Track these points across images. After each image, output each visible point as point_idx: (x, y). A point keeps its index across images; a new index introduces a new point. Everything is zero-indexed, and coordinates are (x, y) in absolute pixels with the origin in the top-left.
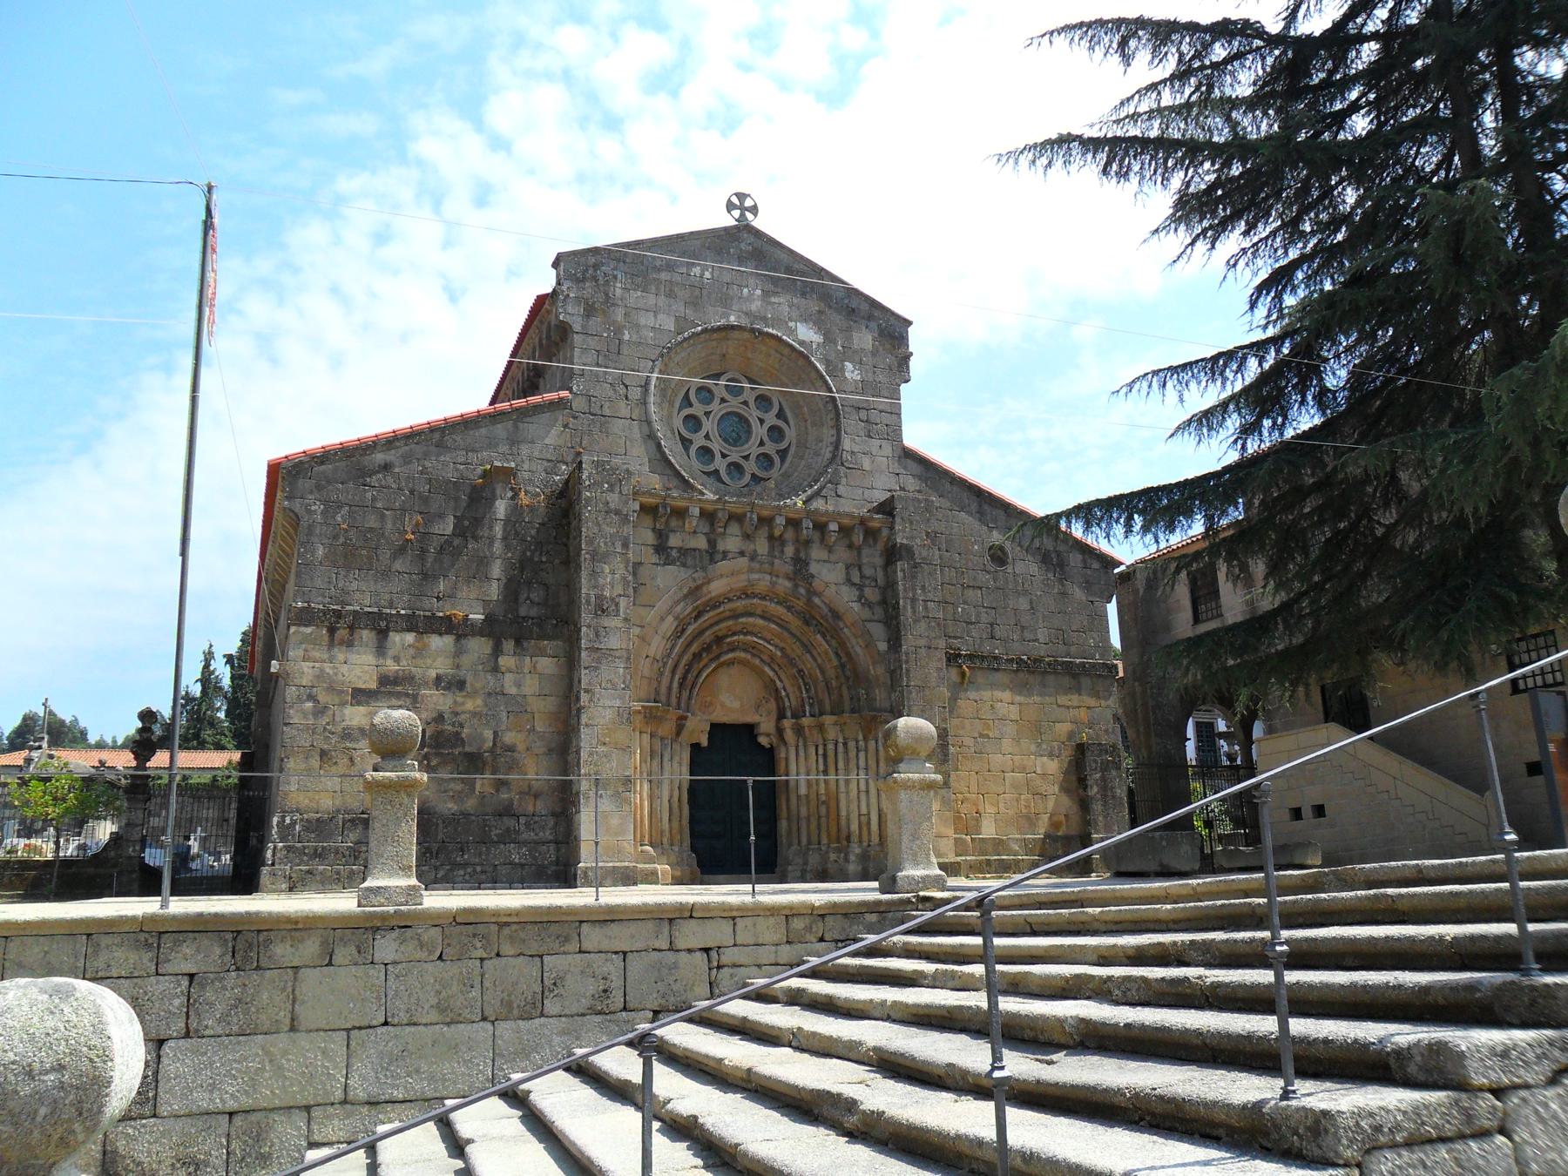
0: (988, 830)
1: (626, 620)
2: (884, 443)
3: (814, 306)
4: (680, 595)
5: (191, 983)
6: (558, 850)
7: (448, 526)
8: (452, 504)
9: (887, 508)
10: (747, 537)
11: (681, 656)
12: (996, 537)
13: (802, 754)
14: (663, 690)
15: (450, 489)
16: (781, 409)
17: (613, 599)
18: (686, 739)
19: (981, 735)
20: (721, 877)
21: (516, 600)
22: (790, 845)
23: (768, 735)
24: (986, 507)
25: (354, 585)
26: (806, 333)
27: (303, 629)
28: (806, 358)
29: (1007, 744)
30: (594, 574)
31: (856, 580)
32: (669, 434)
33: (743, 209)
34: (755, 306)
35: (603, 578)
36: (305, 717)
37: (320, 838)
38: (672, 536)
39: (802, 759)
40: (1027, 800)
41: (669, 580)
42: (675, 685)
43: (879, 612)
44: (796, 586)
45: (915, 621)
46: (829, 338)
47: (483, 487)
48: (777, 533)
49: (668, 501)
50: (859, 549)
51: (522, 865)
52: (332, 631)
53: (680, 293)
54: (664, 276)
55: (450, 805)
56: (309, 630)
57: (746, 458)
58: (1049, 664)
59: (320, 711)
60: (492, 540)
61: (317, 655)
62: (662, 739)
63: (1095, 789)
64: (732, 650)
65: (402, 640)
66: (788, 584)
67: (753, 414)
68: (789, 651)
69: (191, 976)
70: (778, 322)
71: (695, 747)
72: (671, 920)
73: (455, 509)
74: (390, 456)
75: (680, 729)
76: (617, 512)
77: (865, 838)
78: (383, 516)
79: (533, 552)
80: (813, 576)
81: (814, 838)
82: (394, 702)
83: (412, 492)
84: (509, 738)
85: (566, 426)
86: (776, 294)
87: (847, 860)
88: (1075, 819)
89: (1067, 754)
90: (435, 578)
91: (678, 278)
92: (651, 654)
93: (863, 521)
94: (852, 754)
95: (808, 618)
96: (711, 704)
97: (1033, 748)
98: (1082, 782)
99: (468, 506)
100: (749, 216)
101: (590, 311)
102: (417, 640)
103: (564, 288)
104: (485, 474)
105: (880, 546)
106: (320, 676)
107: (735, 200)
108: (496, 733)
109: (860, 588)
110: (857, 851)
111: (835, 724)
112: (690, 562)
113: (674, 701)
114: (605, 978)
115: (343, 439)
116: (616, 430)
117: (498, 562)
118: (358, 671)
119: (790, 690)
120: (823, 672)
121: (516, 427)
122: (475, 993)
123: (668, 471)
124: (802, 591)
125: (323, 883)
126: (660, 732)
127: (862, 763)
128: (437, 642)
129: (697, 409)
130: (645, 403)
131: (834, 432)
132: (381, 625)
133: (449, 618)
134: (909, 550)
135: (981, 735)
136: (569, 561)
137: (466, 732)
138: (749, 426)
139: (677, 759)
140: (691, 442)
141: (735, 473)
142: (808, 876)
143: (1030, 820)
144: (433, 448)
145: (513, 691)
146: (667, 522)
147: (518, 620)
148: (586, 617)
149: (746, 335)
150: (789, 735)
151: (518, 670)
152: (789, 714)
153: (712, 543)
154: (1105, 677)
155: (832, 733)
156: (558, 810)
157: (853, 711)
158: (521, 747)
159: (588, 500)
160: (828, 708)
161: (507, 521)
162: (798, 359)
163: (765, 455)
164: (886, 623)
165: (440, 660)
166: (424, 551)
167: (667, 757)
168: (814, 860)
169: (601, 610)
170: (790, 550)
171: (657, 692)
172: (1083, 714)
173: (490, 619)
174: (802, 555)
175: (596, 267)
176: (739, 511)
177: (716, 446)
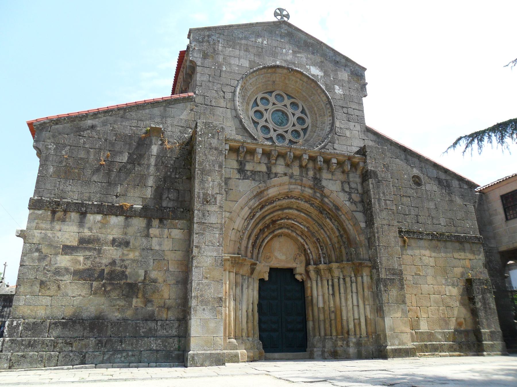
0: (424, 327)
1: (221, 207)
2: (356, 124)
3: (318, 59)
4: (252, 195)
6: (179, 341)
7: (124, 158)
8: (128, 146)
9: (362, 152)
10: (288, 165)
11: (253, 230)
12: (415, 171)
13: (320, 284)
14: (243, 248)
15: (126, 139)
17: (213, 196)
18: (256, 276)
19: (416, 274)
20: (276, 355)
21: (161, 198)
22: (314, 336)
23: (301, 274)
24: (409, 157)
25: (69, 188)
26: (315, 71)
27: (36, 211)
28: (315, 82)
29: (430, 279)
30: (202, 181)
31: (347, 189)
32: (246, 118)
34: (289, 57)
35: (208, 183)
36: (33, 261)
37: (34, 335)
38: (247, 164)
39: (320, 284)
40: (443, 310)
41: (245, 188)
42: (250, 245)
43: (360, 207)
45: (381, 211)
46: (326, 74)
47: (145, 138)
48: (304, 164)
49: (245, 145)
50: (348, 174)
51: (157, 351)
52: (54, 212)
53: (251, 50)
54: (243, 42)
55: (116, 314)
56: (40, 212)
57: (286, 132)
58: (448, 237)
60: (149, 166)
61: (43, 226)
62: (242, 276)
64: (281, 228)
66: (311, 191)
67: (289, 111)
68: (311, 228)
70: (300, 65)
71: (261, 281)
73: (129, 149)
74: (95, 122)
75: (253, 271)
76: (216, 149)
78: (88, 152)
79: (171, 173)
80: (324, 187)
81: (328, 332)
82: (190, 265)
83: (106, 140)
84: (154, 275)
85: (192, 110)
87: (348, 346)
88: (470, 320)
89: (462, 284)
90: (116, 185)
91: (251, 43)
92: (236, 228)
93: (349, 158)
94: (348, 285)
95: (322, 210)
96: (270, 257)
97: (444, 281)
98: (472, 300)
99: (137, 148)
101: (205, 56)
103: (193, 45)
104: (147, 132)
105: (359, 172)
106: (45, 238)
107: (278, 11)
108: (146, 272)
109: (350, 194)
110: (354, 340)
111: (338, 268)
112: (257, 178)
113: (249, 254)
115: (69, 112)
116: (218, 113)
117: (152, 177)
119: (312, 249)
120: (330, 240)
121: (165, 110)
123: (246, 134)
124: (318, 195)
125: (31, 363)
126: (241, 272)
127: (354, 290)
128: (115, 220)
129: (261, 108)
130: (234, 101)
131: (331, 118)
132: (82, 211)
133: (121, 207)
134: (375, 173)
135: (416, 274)
137: (128, 271)
139: (251, 287)
140: (258, 123)
142: (326, 355)
143: (446, 321)
144: (119, 119)
145: (157, 248)
146: (244, 157)
147: (161, 209)
148: (197, 205)
149: (285, 71)
150: (312, 274)
151: (161, 236)
152: (312, 263)
153: (269, 169)
154: (477, 243)
155: (336, 273)
156: (181, 317)
157: (348, 260)
158: (160, 280)
159: (200, 142)
160: (334, 259)
161: (158, 156)
162: (312, 82)
163: (296, 131)
164: (364, 213)
165: (115, 230)
166: (110, 171)
167: (245, 286)
169: (206, 201)
170: (311, 173)
171: (239, 249)
172: (467, 263)
173: (145, 208)
174: (318, 176)
175: (209, 36)
176: (283, 151)
177: (271, 126)
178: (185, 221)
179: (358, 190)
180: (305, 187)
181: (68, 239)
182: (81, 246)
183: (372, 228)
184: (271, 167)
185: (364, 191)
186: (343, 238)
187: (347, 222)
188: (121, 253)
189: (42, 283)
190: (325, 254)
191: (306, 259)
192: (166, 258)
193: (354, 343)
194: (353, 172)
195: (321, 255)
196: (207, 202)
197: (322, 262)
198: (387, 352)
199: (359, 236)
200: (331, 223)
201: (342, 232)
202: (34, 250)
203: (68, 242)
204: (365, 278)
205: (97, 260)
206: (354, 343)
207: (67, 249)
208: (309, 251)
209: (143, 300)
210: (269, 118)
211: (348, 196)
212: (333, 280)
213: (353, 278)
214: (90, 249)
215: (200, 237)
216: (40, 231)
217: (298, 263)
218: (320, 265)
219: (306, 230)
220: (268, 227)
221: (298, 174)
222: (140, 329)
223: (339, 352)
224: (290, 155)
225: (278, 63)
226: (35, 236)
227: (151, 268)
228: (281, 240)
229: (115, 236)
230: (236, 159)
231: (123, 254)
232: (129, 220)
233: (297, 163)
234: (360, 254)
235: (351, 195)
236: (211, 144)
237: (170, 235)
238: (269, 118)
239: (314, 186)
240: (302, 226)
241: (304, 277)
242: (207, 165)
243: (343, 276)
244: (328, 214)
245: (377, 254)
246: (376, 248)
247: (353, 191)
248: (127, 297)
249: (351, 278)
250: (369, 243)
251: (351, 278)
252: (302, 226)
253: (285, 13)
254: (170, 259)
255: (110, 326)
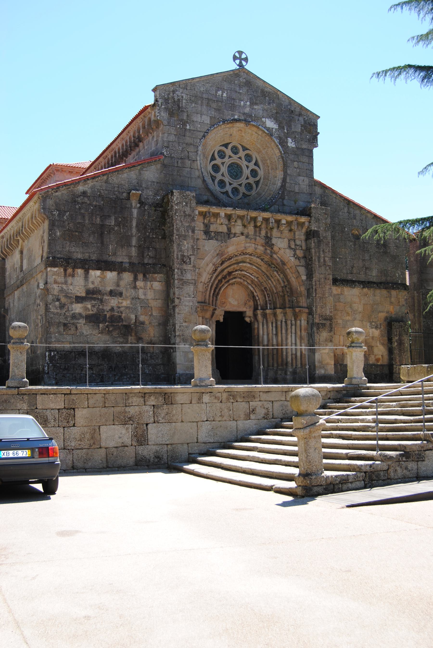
5: (154, 408)
10: (244, 226)
11: (214, 281)
13: (265, 326)
16: (256, 161)
21: (143, 256)
23: (250, 317)
31: (293, 247)
33: (241, 59)
34: (247, 110)
39: (265, 326)
43: (303, 262)
44: (266, 249)
45: (320, 266)
48: (259, 224)
56: (56, 269)
57: (240, 185)
59: (62, 306)
63: (396, 344)
64: (235, 278)
65: (95, 274)
69: (153, 406)
72: (286, 392)
77: (294, 364)
79: (150, 233)
80: (273, 245)
84: (142, 318)
86: (256, 104)
87: (286, 374)
88: (386, 357)
92: (203, 281)
100: (244, 63)
102: (102, 274)
105: (304, 230)
106: (62, 290)
108: (136, 316)
109: (295, 250)
110: (291, 370)
112: (219, 238)
114: (267, 409)
118: (77, 288)
122: (231, 412)
124: (269, 252)
136: (167, 237)
138: (242, 169)
141: (236, 193)
142: (268, 381)
150: (260, 317)
151: (145, 288)
152: (260, 308)
153: (229, 229)
155: (280, 317)
158: (147, 322)
163: (249, 184)
168: (271, 374)
170: (263, 233)
174: (269, 235)
175: (174, 92)
177: (227, 179)
178: (162, 275)
179: (302, 247)
180: (258, 245)
181: (78, 291)
182: (88, 296)
183: (311, 281)
184: (230, 228)
185: (307, 248)
186: (287, 288)
187: (291, 275)
188: (117, 302)
189: (65, 325)
190: (271, 301)
191: (254, 305)
192: (150, 306)
193: (290, 372)
194: (299, 230)
195: (268, 302)
196: (184, 262)
197: (268, 308)
198: (315, 378)
199: (300, 287)
200: (277, 276)
201: (286, 283)
202: (56, 300)
203: (79, 293)
204: (303, 322)
205: (101, 307)
206: (290, 372)
207: (79, 299)
208: (257, 298)
209: (135, 337)
210: (225, 171)
211: (293, 253)
212: (276, 323)
213: (293, 322)
214: (94, 299)
215: (180, 290)
216: (58, 285)
217: (248, 308)
218: (267, 310)
219: (256, 280)
220: (225, 278)
221: (253, 234)
222: (136, 359)
223: (279, 379)
224: (247, 218)
225: (236, 117)
226: (54, 289)
227: (139, 313)
228: (234, 288)
229: (112, 288)
230: (203, 221)
231: (119, 302)
232: (121, 275)
233: (252, 224)
234: (300, 302)
235: (296, 251)
236: (185, 211)
237: (152, 286)
238: (225, 171)
239: (266, 244)
240: (252, 277)
241: (253, 320)
242: (183, 231)
243: (285, 320)
244: (275, 268)
245: (313, 303)
246: (313, 298)
247: (298, 248)
248: (124, 335)
249: (291, 321)
250: (308, 293)
251: (291, 321)
252: (252, 277)
253: (243, 56)
254: (153, 306)
255: (115, 357)
